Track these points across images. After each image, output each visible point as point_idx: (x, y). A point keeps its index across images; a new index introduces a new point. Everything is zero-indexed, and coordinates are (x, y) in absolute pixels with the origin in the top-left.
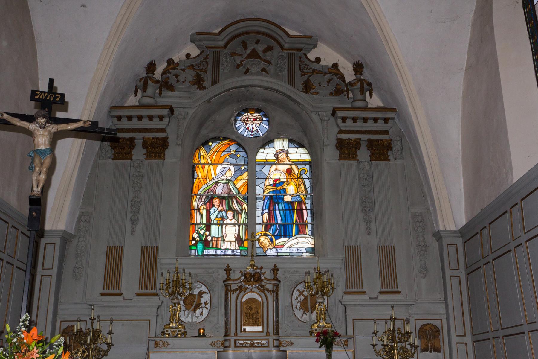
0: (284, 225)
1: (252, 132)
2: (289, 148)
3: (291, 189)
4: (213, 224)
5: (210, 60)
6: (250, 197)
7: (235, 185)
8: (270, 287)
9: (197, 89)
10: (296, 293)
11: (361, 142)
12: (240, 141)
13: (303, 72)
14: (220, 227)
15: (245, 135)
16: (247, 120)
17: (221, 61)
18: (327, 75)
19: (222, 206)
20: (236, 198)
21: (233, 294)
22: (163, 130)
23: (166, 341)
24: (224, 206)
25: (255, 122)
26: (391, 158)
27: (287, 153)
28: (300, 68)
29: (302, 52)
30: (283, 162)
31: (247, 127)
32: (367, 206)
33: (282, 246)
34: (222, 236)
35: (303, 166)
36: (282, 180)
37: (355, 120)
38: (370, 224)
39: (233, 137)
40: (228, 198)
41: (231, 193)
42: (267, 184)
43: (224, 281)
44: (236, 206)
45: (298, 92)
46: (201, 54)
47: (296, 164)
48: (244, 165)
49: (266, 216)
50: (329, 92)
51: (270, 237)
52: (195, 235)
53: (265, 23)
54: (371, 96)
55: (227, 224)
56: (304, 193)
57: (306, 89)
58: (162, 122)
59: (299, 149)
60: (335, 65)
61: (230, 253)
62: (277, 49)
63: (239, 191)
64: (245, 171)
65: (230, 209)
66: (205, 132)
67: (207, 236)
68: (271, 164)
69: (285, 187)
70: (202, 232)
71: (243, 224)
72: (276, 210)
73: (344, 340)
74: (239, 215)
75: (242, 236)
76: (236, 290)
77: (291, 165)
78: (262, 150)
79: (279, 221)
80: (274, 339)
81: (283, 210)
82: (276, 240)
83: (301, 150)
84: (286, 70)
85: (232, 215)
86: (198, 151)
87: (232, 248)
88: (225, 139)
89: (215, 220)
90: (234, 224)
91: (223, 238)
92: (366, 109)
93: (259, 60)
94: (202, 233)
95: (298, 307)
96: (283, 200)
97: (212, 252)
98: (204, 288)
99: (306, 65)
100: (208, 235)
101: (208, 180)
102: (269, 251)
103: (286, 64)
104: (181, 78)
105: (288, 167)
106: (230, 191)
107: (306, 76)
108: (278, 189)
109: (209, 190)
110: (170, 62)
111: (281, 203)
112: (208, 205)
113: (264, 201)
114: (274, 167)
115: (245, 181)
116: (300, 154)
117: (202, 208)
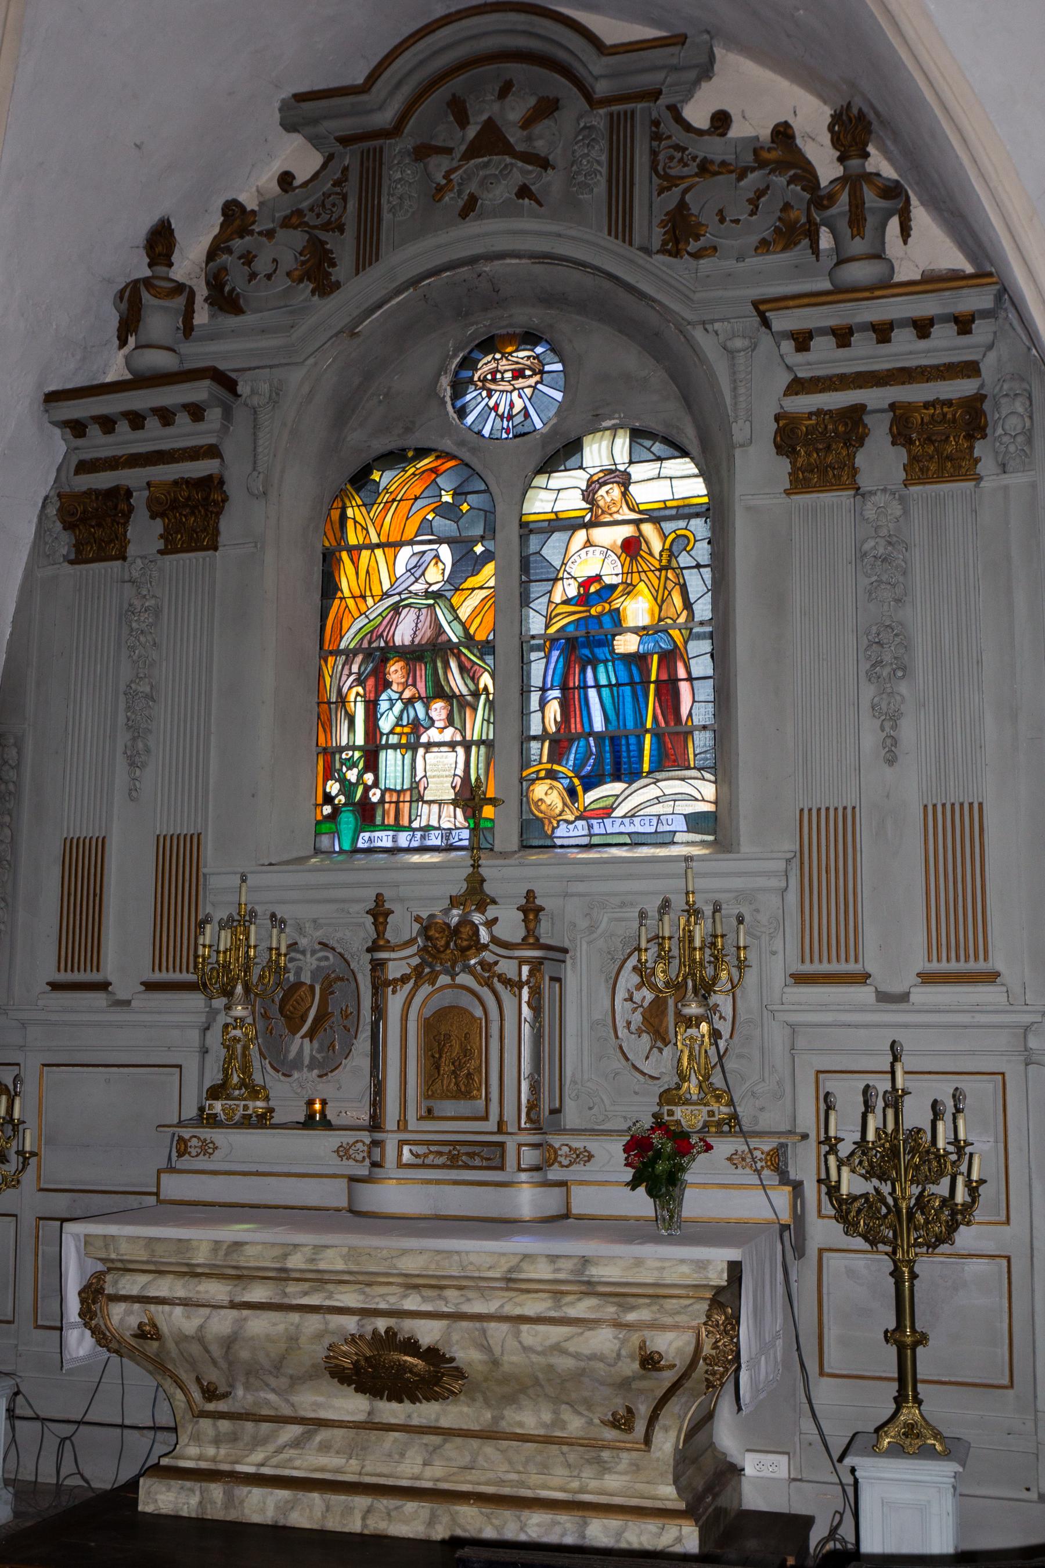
0: (612, 739)
1: (510, 417)
2: (631, 462)
3: (638, 610)
4: (388, 746)
5: (352, 186)
7: (453, 610)
9: (313, 292)
11: (867, 419)
12: (467, 457)
13: (666, 177)
14: (408, 756)
15: (486, 432)
16: (494, 380)
17: (385, 183)
18: (752, 177)
19: (414, 685)
20: (458, 656)
21: (394, 992)
22: (212, 452)
23: (208, 1137)
24: (421, 685)
25: (520, 383)
26: (986, 466)
27: (625, 481)
28: (654, 167)
29: (663, 101)
31: (492, 404)
32: (886, 655)
33: (607, 812)
34: (415, 786)
35: (682, 524)
36: (608, 580)
37: (843, 336)
38: (895, 727)
39: (447, 444)
40: (429, 653)
41: (443, 638)
42: (557, 598)
43: (369, 950)
44: (457, 683)
45: (641, 257)
46: (324, 166)
47: (656, 516)
48: (482, 538)
49: (554, 709)
50: (754, 239)
51: (566, 782)
52: (333, 787)
53: (522, 17)
54: (906, 232)
55: (429, 746)
56: (682, 620)
57: (677, 242)
58: (201, 426)
59: (667, 464)
60: (783, 133)
61: (438, 842)
62: (574, 103)
63: (466, 630)
64: (488, 556)
65: (440, 692)
66: (362, 439)
67: (367, 789)
68: (572, 525)
69: (616, 604)
70: (352, 775)
71: (481, 742)
72: (586, 687)
73: (766, 1148)
74: (468, 712)
76: (404, 979)
77: (637, 523)
78: (540, 480)
79: (598, 725)
80: (520, 1145)
81: (610, 685)
82: (586, 790)
83: (684, 466)
84: (603, 181)
85: (444, 714)
86: (338, 504)
87: (445, 825)
88: (422, 453)
89: (392, 732)
90: (452, 745)
91: (416, 794)
92: (887, 286)
93: (508, 159)
94: (354, 780)
95: (633, 1027)
96: (612, 651)
97: (384, 839)
99: (678, 148)
100: (370, 783)
101: (370, 601)
102: (562, 831)
103: (604, 158)
104: (262, 265)
105: (628, 531)
106: (439, 630)
107: (677, 191)
108: (593, 612)
109: (374, 634)
110: (232, 210)
111: (605, 662)
112: (371, 682)
113: (548, 657)
114: (581, 536)
115: (484, 593)
116: (677, 481)
117: (352, 697)
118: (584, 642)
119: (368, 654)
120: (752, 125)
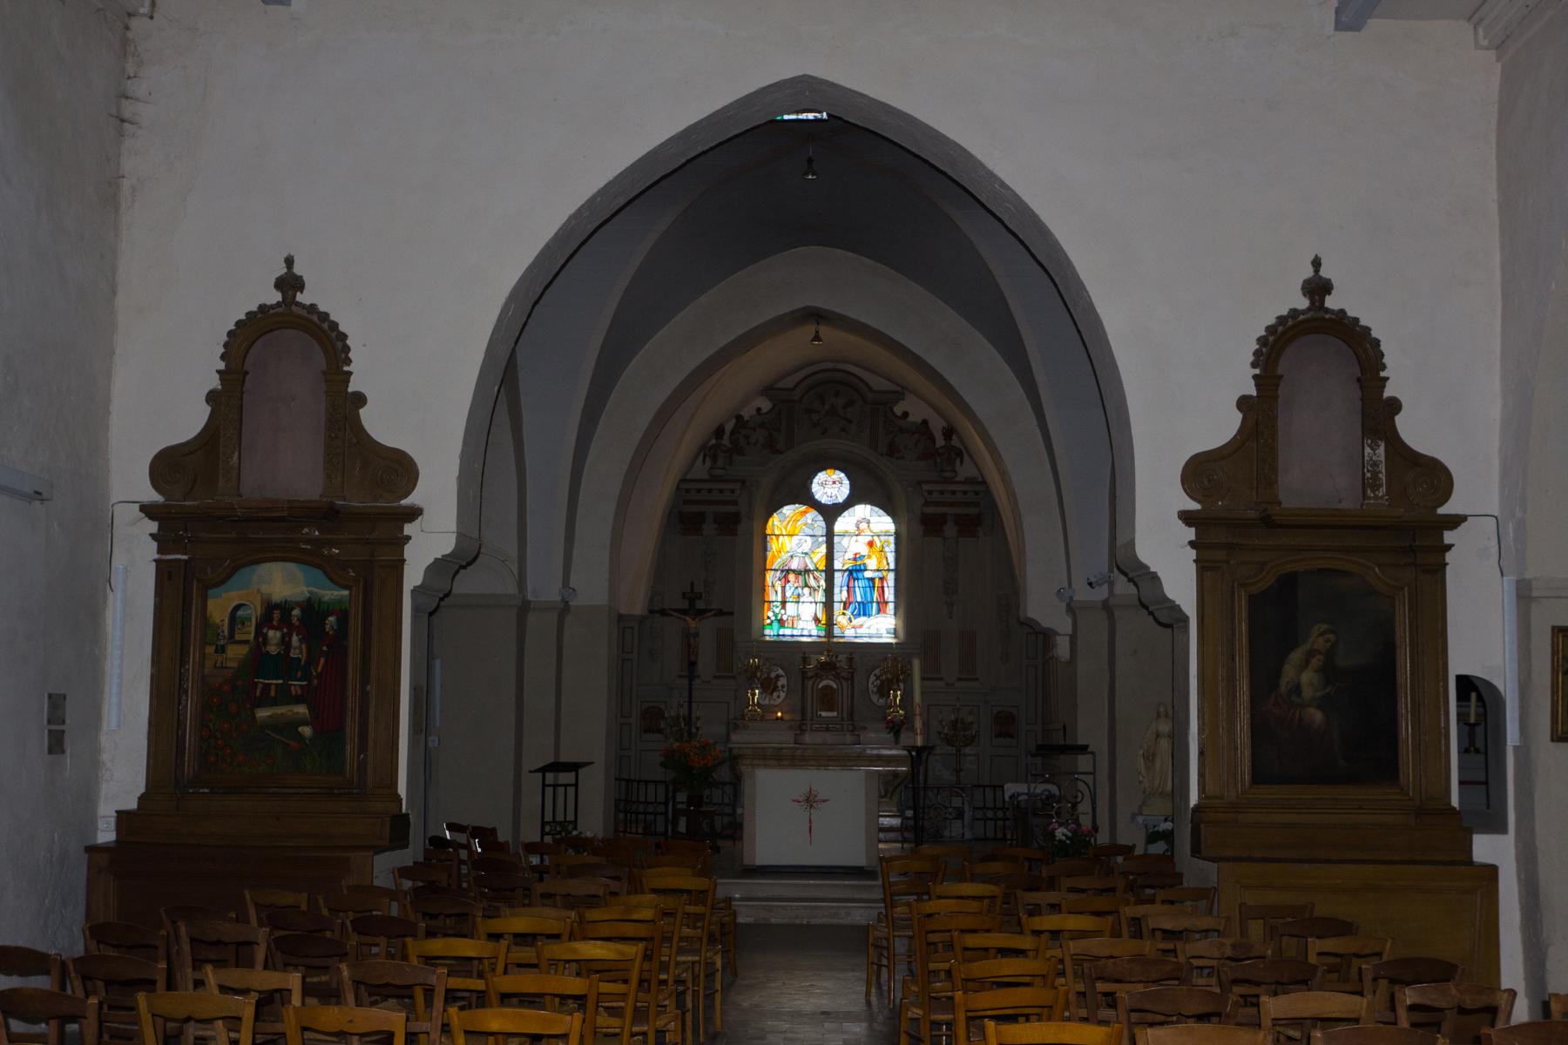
3: (872, 563)
6: (829, 572)
8: (844, 674)
10: (872, 678)
30: (869, 533)
44: (812, 582)
52: (770, 614)
60: (925, 422)
75: (820, 615)
98: (780, 672)
120: (915, 417)
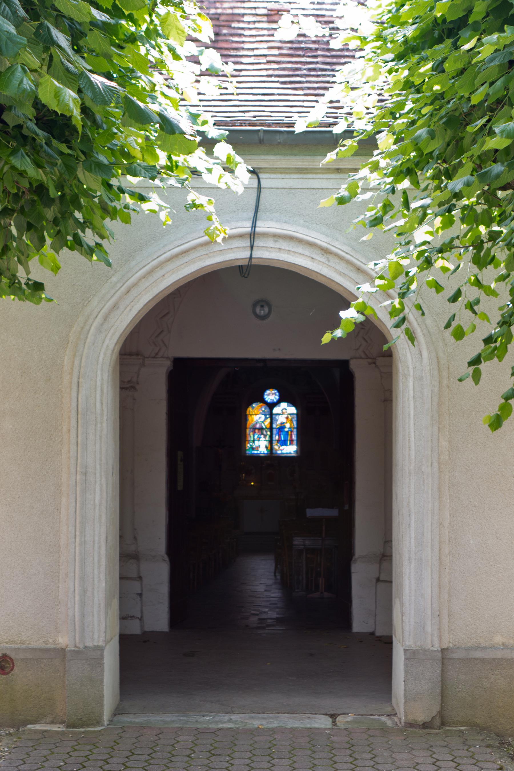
3: (288, 425)
6: (271, 429)
44: (265, 433)
47: (290, 414)
118: (282, 428)
119: (253, 428)
